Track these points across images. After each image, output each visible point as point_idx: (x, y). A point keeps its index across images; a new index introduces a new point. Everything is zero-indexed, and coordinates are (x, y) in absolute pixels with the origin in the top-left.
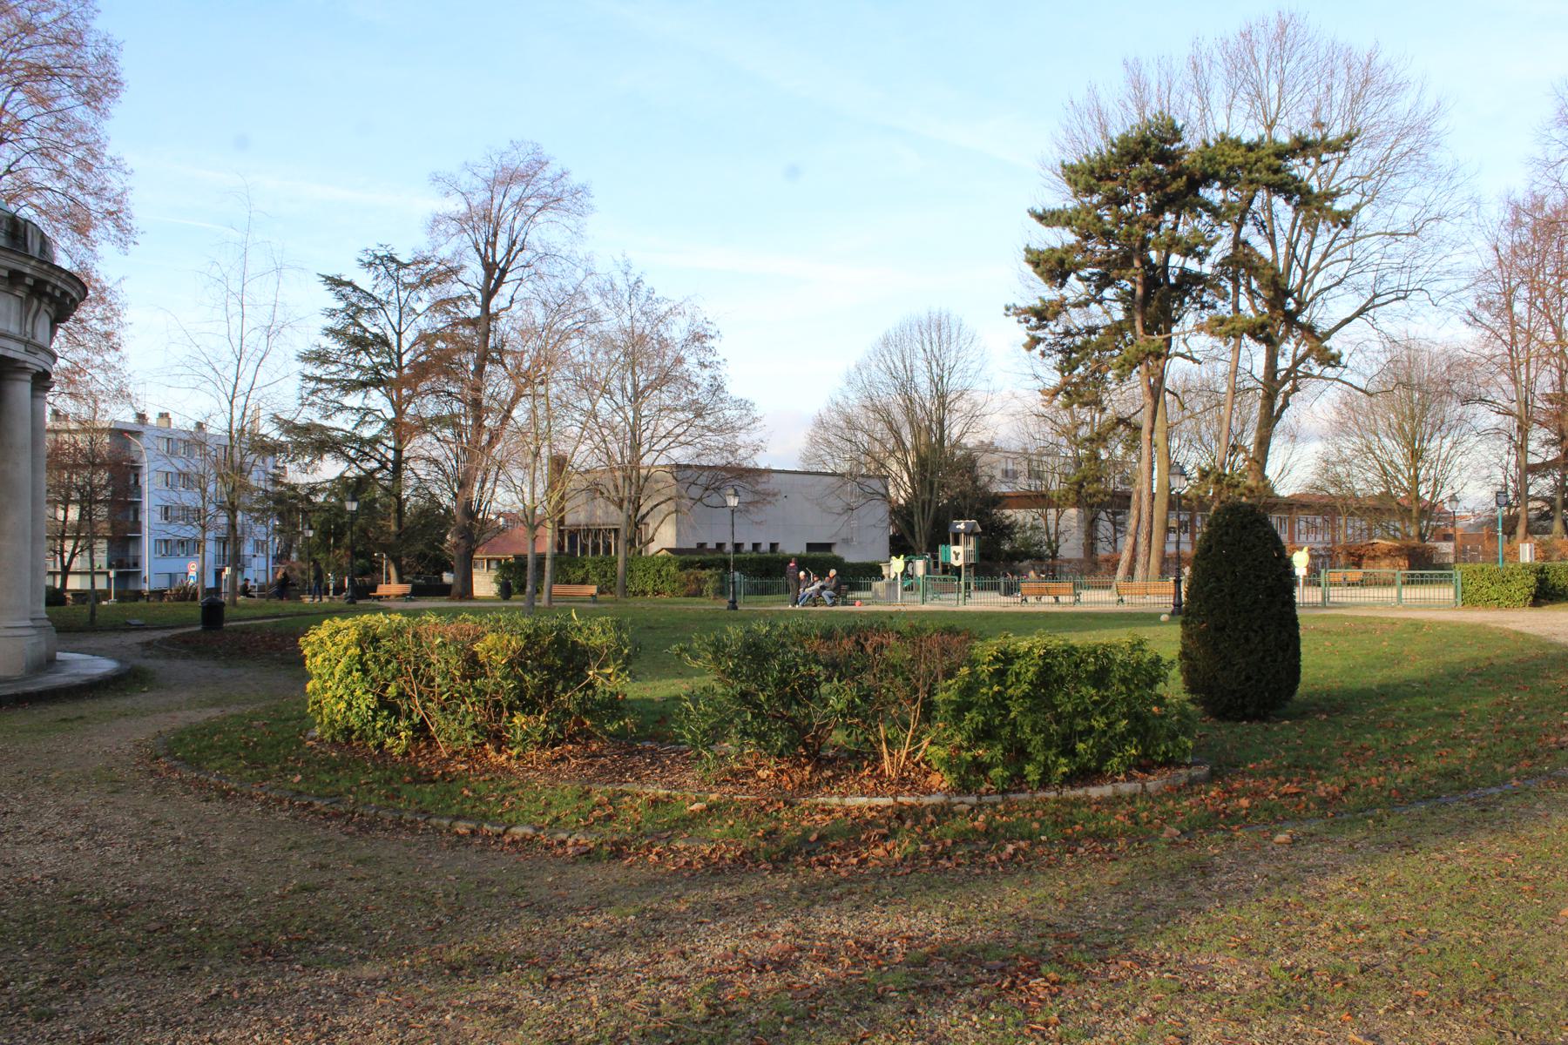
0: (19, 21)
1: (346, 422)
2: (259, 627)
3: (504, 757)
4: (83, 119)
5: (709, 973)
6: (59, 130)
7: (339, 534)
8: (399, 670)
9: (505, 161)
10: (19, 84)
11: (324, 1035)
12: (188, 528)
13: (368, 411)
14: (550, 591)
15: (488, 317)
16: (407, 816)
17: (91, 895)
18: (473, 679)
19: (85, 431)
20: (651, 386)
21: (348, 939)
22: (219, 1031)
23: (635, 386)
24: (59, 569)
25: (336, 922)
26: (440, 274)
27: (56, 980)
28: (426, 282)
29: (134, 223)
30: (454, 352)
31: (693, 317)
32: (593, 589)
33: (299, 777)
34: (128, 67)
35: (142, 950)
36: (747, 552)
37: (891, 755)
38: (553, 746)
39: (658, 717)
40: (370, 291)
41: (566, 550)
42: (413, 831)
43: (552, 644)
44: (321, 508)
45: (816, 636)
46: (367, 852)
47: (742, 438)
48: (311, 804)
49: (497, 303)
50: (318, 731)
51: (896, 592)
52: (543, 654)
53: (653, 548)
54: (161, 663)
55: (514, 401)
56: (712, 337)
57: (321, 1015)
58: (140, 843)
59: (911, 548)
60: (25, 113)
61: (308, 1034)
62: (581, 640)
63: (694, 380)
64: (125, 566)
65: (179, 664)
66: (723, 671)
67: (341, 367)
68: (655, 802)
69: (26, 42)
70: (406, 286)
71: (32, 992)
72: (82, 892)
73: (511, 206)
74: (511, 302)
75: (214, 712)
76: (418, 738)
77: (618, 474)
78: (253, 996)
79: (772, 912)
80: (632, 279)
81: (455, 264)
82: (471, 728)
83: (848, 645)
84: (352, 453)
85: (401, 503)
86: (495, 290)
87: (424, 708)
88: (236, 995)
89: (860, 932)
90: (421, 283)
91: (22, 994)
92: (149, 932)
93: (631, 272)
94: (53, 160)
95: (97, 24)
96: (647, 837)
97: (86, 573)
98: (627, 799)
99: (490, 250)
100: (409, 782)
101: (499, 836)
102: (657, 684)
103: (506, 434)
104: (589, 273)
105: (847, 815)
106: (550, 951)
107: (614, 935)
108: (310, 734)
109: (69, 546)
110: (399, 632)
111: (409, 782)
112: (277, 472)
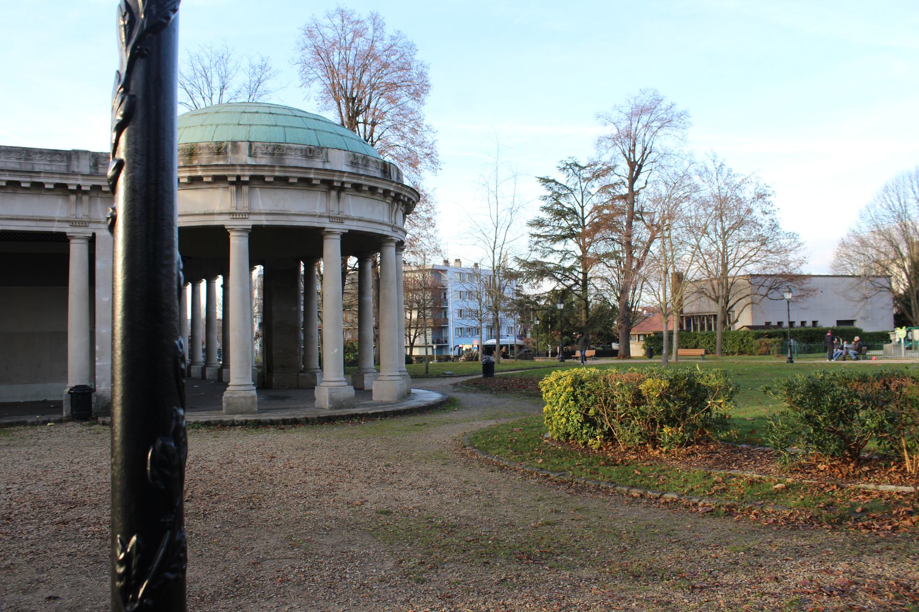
0: (381, 62)
1: (555, 259)
2: (513, 375)
3: (658, 452)
4: (412, 107)
5: (795, 593)
6: (401, 114)
7: (553, 322)
8: (596, 400)
9: (638, 102)
10: (382, 94)
11: (564, 608)
12: (473, 321)
13: (568, 252)
14: (677, 353)
15: (633, 193)
16: (603, 485)
17: (437, 519)
18: (639, 405)
19: (420, 271)
20: (733, 228)
21: (573, 554)
22: (507, 599)
23: (723, 228)
24: (408, 344)
25: (566, 544)
26: (604, 171)
27: (423, 563)
28: (596, 176)
29: (439, 158)
30: (614, 215)
31: (758, 184)
32: (702, 351)
33: (541, 460)
34: (433, 77)
35: (464, 551)
36: (797, 327)
37: (911, 458)
38: (686, 446)
39: (750, 430)
40: (565, 184)
41: (685, 328)
42: (606, 492)
43: (685, 385)
44: (543, 308)
45: (855, 380)
46: (581, 504)
47: (792, 256)
48: (548, 476)
49: (637, 185)
50: (550, 434)
51: (900, 351)
52: (680, 391)
53: (738, 326)
54: (463, 395)
55: (651, 241)
56: (769, 195)
57: (561, 596)
58: (459, 493)
59: (910, 322)
60: (385, 108)
61: (555, 606)
62: (703, 383)
63: (760, 222)
64: (441, 343)
65: (472, 396)
66: (794, 402)
67: (551, 228)
68: (752, 482)
69: (385, 72)
70: (585, 179)
71: (413, 568)
72: (433, 517)
73: (643, 127)
74: (646, 184)
75: (492, 422)
76: (607, 439)
77: (715, 282)
78: (524, 581)
79: (833, 556)
80: (718, 164)
81: (612, 165)
82: (637, 434)
83: (878, 385)
84: (559, 276)
85: (587, 303)
86: (636, 178)
87: (610, 422)
88: (515, 580)
89: (898, 576)
90: (593, 177)
91: (408, 568)
92: (467, 541)
93: (717, 159)
94: (399, 130)
95: (416, 57)
96: (748, 503)
97: (424, 346)
98: (734, 479)
99: (632, 155)
100: (603, 465)
101: (657, 498)
102: (747, 409)
103: (647, 260)
104: (692, 163)
105: (881, 496)
106: (692, 570)
107: (731, 563)
108: (546, 436)
109: (413, 332)
110: (595, 378)
111: (603, 465)
112: (518, 288)
